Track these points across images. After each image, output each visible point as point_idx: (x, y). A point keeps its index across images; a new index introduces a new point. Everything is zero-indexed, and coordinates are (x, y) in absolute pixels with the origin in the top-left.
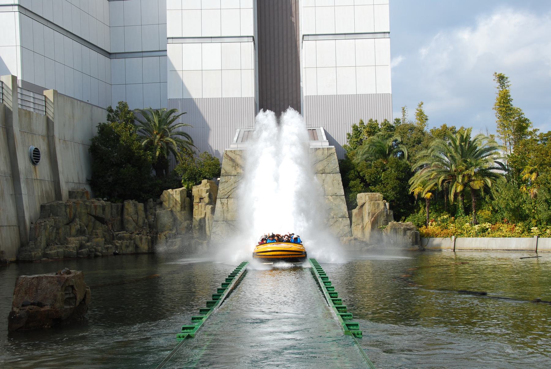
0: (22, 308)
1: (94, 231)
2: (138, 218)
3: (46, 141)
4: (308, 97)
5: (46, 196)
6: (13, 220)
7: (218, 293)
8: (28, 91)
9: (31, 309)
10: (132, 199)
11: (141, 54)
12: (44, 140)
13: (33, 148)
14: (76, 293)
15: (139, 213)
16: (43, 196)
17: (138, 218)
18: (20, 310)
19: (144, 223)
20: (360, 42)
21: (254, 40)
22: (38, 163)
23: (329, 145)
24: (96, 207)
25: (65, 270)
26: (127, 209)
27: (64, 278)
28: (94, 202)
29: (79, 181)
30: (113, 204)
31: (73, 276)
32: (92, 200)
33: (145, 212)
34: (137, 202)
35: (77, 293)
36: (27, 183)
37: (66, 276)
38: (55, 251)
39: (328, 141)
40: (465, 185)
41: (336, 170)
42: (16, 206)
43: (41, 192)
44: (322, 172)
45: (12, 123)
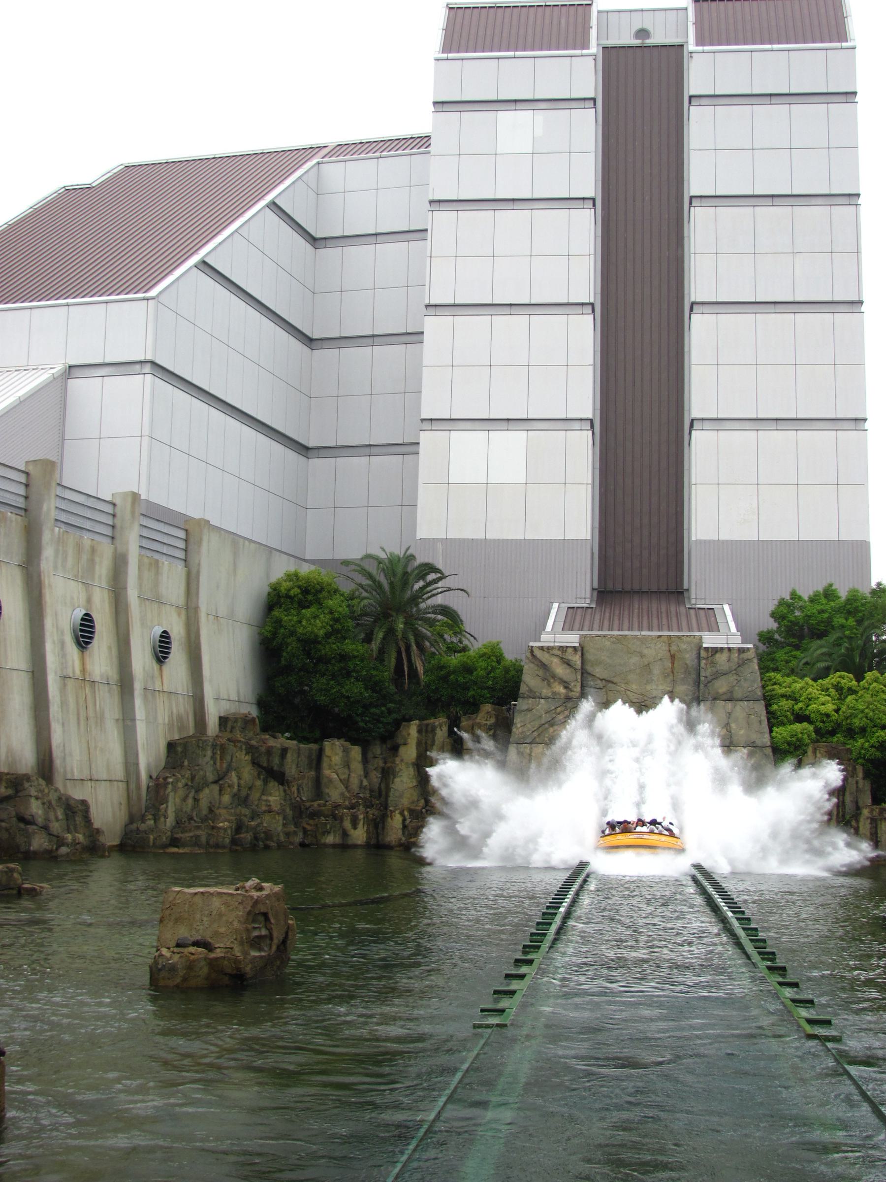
0: (176, 950)
1: (264, 798)
2: (349, 775)
3: (183, 617)
4: (705, 543)
5: (178, 725)
6: (119, 772)
7: (531, 942)
8: (158, 520)
9: (193, 954)
10: (339, 738)
11: (367, 450)
12: (179, 615)
13: (158, 631)
14: (272, 929)
15: (353, 767)
16: (173, 725)
17: (349, 775)
18: (174, 953)
19: (361, 786)
20: (806, 437)
21: (592, 426)
22: (167, 660)
23: (742, 643)
24: (269, 752)
25: (252, 882)
26: (329, 757)
27: (252, 897)
28: (267, 739)
29: (239, 696)
30: (302, 746)
31: (267, 895)
32: (263, 737)
33: (364, 764)
34: (347, 744)
35: (273, 926)
36: (145, 698)
37: (256, 894)
38: (191, 834)
39: (739, 633)
40: (801, 689)
41: (756, 693)
42: (125, 743)
43: (169, 717)
44: (725, 697)
45: (126, 582)
